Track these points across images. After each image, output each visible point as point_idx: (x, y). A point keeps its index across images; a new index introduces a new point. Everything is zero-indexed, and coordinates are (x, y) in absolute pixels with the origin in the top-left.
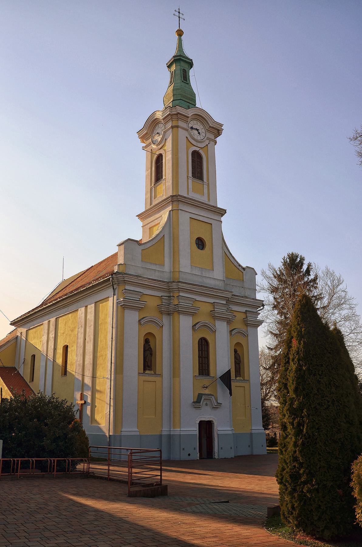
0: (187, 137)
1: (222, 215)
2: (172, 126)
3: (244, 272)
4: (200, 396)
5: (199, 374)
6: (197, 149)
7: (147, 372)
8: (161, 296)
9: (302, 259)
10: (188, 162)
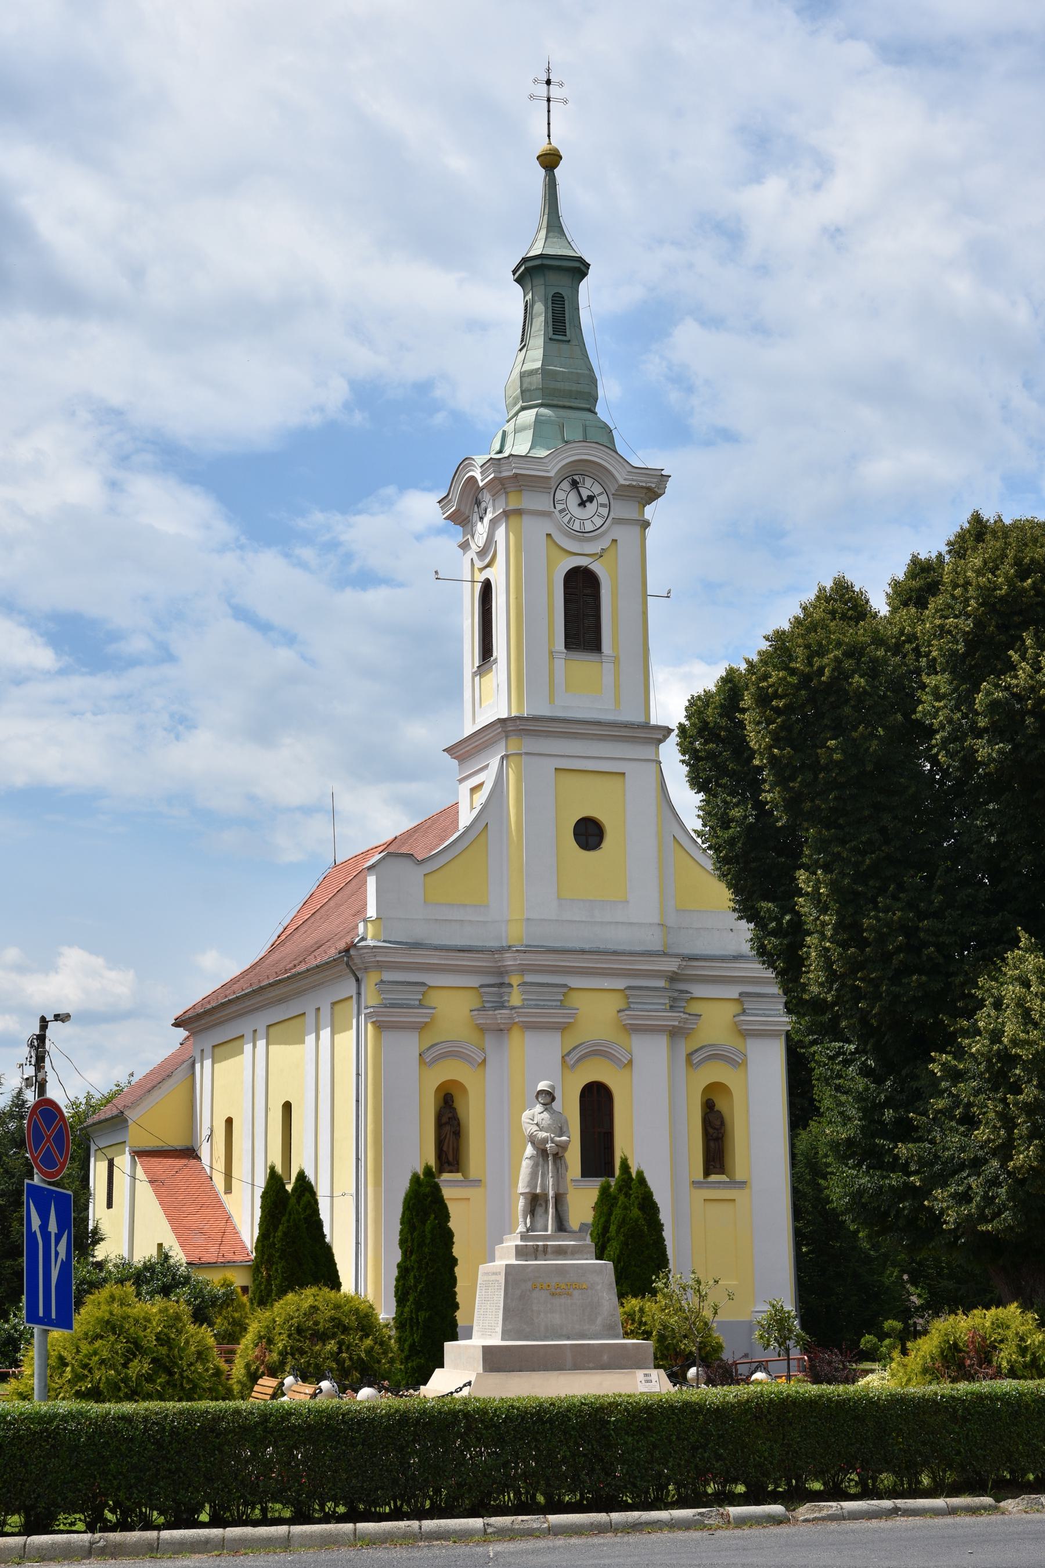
2: (504, 512)
5: (583, 1176)
7: (713, 1178)
8: (482, 986)
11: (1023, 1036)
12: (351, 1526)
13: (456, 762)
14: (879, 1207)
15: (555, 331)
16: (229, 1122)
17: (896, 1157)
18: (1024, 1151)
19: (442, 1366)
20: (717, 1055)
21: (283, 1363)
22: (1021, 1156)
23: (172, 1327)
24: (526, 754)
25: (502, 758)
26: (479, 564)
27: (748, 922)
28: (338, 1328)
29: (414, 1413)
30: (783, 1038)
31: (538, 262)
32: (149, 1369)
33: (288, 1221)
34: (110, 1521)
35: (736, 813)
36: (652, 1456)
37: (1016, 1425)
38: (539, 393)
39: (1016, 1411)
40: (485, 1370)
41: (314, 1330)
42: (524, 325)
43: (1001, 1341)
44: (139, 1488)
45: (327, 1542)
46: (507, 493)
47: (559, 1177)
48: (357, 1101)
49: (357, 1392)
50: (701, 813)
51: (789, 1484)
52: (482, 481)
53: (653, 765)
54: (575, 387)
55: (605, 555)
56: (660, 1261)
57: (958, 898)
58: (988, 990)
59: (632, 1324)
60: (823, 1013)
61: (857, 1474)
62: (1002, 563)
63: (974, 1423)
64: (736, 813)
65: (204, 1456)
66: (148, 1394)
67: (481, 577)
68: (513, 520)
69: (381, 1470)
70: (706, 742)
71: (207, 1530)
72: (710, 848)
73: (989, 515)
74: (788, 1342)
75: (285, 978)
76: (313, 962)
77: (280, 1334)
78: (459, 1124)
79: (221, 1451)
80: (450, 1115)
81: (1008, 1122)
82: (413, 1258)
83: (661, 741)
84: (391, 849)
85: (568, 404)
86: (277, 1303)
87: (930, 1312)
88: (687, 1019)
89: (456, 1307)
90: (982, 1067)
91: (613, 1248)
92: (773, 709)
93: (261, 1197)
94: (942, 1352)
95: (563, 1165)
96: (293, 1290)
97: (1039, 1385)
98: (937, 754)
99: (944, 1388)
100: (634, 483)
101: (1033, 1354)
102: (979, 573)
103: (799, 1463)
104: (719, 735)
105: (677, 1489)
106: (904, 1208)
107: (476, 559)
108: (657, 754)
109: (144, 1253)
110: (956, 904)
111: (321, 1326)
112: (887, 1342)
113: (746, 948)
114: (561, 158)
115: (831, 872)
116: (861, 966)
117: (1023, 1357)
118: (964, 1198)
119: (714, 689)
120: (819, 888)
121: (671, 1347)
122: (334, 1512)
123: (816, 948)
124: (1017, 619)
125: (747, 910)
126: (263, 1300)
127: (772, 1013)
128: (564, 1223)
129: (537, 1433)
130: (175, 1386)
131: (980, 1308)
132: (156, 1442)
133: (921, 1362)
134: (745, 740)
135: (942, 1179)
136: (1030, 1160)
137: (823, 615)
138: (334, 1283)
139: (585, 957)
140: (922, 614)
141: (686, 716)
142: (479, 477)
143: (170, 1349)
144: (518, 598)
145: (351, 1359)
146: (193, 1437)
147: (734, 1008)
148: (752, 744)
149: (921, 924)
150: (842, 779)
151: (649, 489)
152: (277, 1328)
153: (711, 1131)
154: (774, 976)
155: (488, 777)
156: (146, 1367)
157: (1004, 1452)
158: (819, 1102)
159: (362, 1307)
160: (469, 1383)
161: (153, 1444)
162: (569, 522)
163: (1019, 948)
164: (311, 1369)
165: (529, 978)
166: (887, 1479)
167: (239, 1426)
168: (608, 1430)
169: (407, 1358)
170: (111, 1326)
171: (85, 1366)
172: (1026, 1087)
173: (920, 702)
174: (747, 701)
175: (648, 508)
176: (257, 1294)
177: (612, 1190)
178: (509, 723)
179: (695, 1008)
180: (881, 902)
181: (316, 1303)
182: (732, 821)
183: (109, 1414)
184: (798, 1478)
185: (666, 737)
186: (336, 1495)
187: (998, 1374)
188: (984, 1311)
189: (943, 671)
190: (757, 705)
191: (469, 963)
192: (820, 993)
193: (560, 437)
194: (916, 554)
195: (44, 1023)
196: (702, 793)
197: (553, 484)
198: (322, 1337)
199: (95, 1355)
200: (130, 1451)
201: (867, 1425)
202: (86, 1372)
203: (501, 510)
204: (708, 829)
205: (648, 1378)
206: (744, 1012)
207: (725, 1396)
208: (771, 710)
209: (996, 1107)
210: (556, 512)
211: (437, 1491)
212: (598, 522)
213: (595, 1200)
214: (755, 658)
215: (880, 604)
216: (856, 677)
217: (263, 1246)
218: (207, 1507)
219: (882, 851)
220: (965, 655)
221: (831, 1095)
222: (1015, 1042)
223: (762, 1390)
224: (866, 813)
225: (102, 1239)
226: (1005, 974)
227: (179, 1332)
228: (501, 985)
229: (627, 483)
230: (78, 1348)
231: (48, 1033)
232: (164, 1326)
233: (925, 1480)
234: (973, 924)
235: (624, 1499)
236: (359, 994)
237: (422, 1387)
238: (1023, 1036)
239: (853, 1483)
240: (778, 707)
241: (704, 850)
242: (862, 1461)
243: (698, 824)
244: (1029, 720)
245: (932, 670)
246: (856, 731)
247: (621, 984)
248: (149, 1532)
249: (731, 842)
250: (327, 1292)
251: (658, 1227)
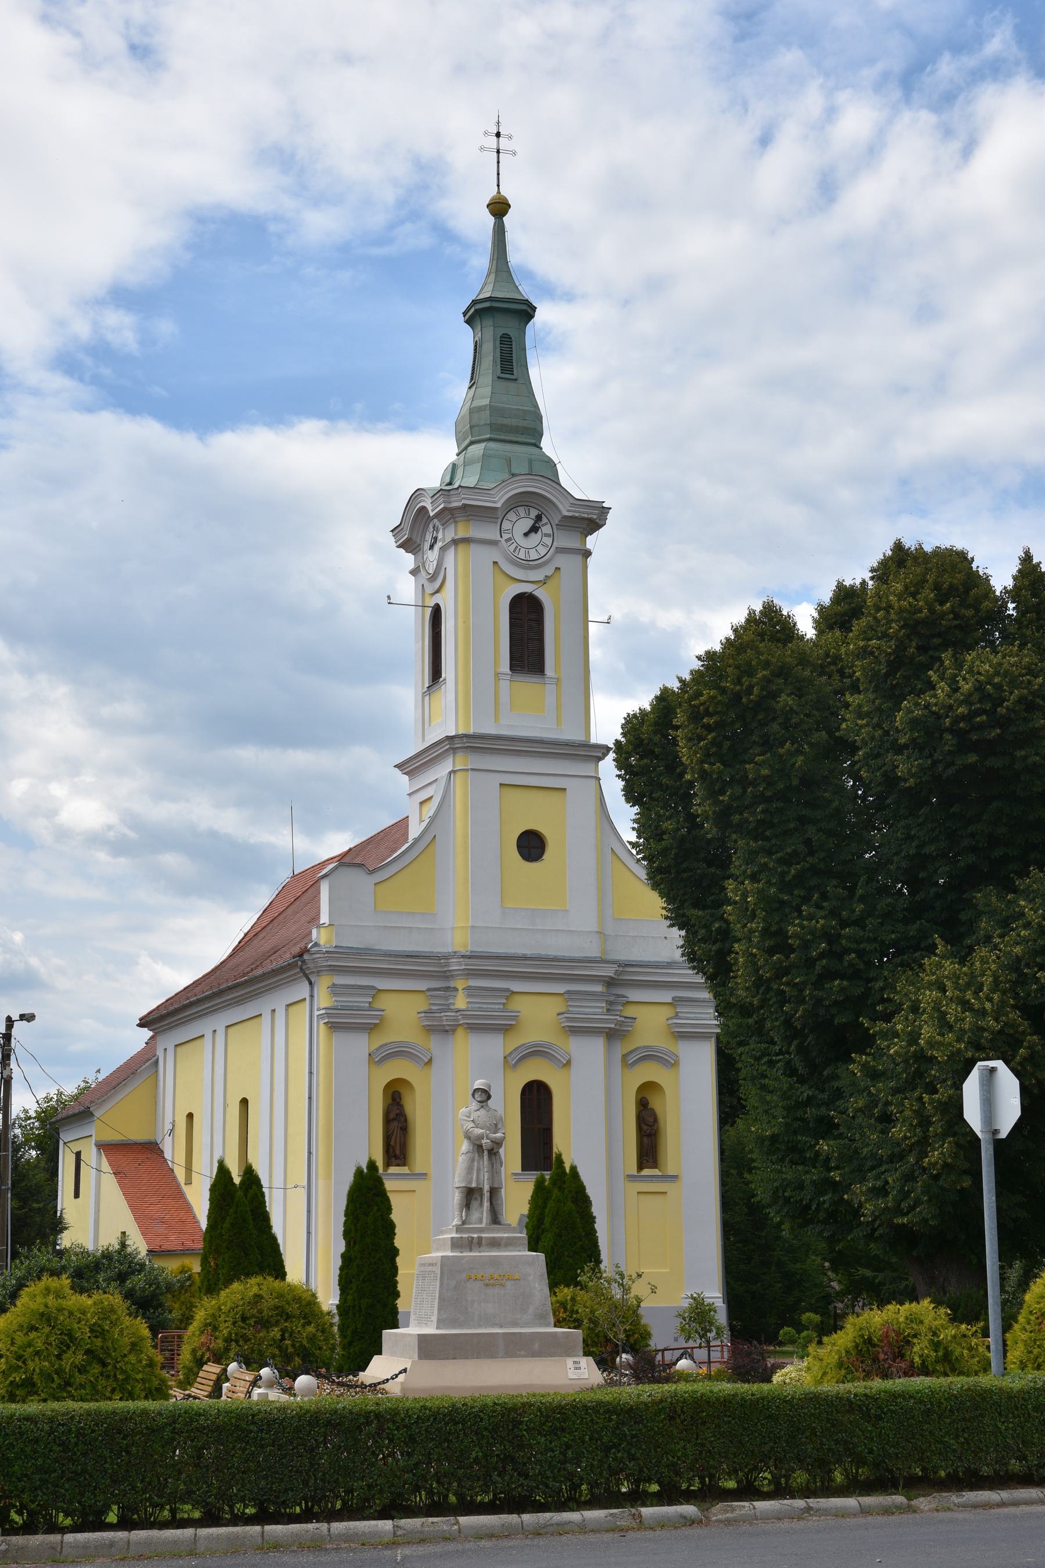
5: (524, 1169)
7: (646, 1172)
8: (429, 990)
11: (939, 1038)
12: (258, 1528)
13: (406, 777)
14: (801, 1200)
15: (503, 371)
16: (190, 1116)
17: (817, 1154)
18: (939, 1147)
19: (380, 1353)
20: (650, 1056)
21: (227, 1349)
22: (936, 1153)
23: (106, 1319)
24: (472, 769)
26: (429, 589)
27: (680, 929)
28: (281, 1316)
29: (326, 1414)
30: (713, 1040)
32: (83, 1360)
33: (236, 1212)
34: (17, 1523)
35: (668, 825)
36: (565, 1455)
37: (929, 1423)
38: (488, 429)
39: (929, 1409)
40: (420, 1357)
41: (257, 1317)
42: (474, 364)
43: (915, 1336)
44: (44, 1490)
45: (235, 1548)
47: (494, 1172)
48: (310, 1098)
49: (294, 1380)
50: (636, 826)
51: (702, 1482)
53: (593, 781)
54: (522, 423)
55: (550, 583)
56: (592, 1254)
57: (879, 907)
58: (906, 994)
59: (565, 1312)
60: (750, 1016)
61: (771, 1472)
62: (923, 588)
63: (887, 1422)
64: (668, 825)
65: (110, 1457)
66: (80, 1384)
67: (431, 602)
68: (461, 548)
69: (290, 1471)
70: (641, 758)
71: (112, 1533)
72: (643, 858)
73: (909, 543)
74: (708, 1334)
75: (242, 982)
76: (269, 967)
77: (226, 1321)
78: (406, 1120)
79: (128, 1452)
80: (398, 1112)
81: (925, 1122)
82: (357, 1247)
83: (600, 759)
84: (346, 860)
85: (514, 439)
86: (222, 1292)
87: (850, 1297)
88: (623, 1022)
89: (397, 1295)
90: (899, 1069)
91: (547, 1239)
92: (703, 726)
93: (210, 1190)
94: (857, 1346)
95: (498, 1161)
96: (239, 1279)
97: (951, 1382)
98: (860, 770)
99: (857, 1387)
100: (577, 514)
101: (945, 1348)
102: (900, 597)
103: (712, 1462)
104: (653, 752)
105: (591, 1490)
106: (824, 1201)
107: (426, 584)
108: (597, 770)
109: (109, 1240)
110: (877, 913)
111: (265, 1313)
112: (805, 1333)
113: (677, 955)
114: (509, 206)
115: (758, 882)
116: (786, 971)
117: (936, 1351)
118: (881, 1191)
119: (649, 708)
120: (747, 897)
121: (602, 1334)
122: (243, 1513)
123: (743, 954)
124: (936, 641)
125: (678, 918)
126: (212, 1285)
127: (703, 1016)
128: (499, 1216)
129: (449, 1433)
130: (108, 1377)
131: (894, 1303)
132: (62, 1444)
133: (836, 1357)
134: (677, 756)
135: (860, 1173)
136: (944, 1156)
137: (752, 636)
138: (279, 1271)
140: (846, 637)
141: (622, 734)
142: (430, 508)
143: (104, 1340)
144: (466, 622)
145: (293, 1346)
146: (100, 1438)
147: (666, 1012)
148: (684, 759)
149: (843, 932)
150: (768, 793)
151: (591, 520)
152: (223, 1316)
153: (645, 1127)
154: (703, 981)
155: (436, 792)
156: (80, 1358)
157: (916, 1449)
158: (745, 1100)
159: (304, 1296)
160: (405, 1370)
161: (59, 1445)
162: (514, 551)
163: (936, 955)
164: (255, 1355)
166: (800, 1477)
167: (147, 1428)
168: (521, 1430)
169: (350, 1343)
170: (46, 1317)
171: (19, 1357)
172: (941, 1087)
173: (844, 720)
174: (680, 718)
175: (589, 538)
176: (205, 1283)
177: (547, 1183)
178: (457, 740)
179: (630, 1011)
180: (805, 910)
181: (261, 1292)
182: (664, 833)
183: (15, 1415)
184: (711, 1477)
185: (605, 755)
186: (244, 1496)
187: (911, 1371)
188: (898, 1306)
189: (866, 690)
190: (689, 722)
192: (747, 997)
193: (507, 471)
194: (841, 581)
195: (10, 1022)
196: (637, 807)
197: (499, 514)
198: (265, 1324)
199: (30, 1347)
200: (35, 1453)
201: (781, 1424)
202: (20, 1364)
204: (642, 840)
205: (578, 1366)
207: (639, 1395)
208: (702, 727)
209: (913, 1105)
210: (503, 540)
211: (350, 1491)
212: (543, 551)
213: (531, 1193)
214: (687, 677)
215: (806, 625)
216: (784, 697)
217: (211, 1236)
218: (115, 1508)
219: (807, 862)
220: (887, 675)
221: (757, 1094)
222: (932, 1044)
223: (676, 1389)
224: (792, 825)
225: (66, 1228)
226: (923, 980)
227: (113, 1324)
228: (447, 989)
229: (570, 514)
230: (13, 1339)
231: (14, 1032)
232: (99, 1318)
233: (838, 1477)
234: (893, 932)
235: (537, 1498)
236: (312, 996)
237: (361, 1373)
238: (939, 1038)
239: (766, 1482)
240: (708, 724)
241: (638, 860)
242: (776, 1460)
243: (633, 837)
244: (948, 736)
245: (855, 689)
246: (783, 748)
247: (561, 988)
248: (52, 1535)
249: (664, 852)
250: (271, 1283)
251: (591, 1220)
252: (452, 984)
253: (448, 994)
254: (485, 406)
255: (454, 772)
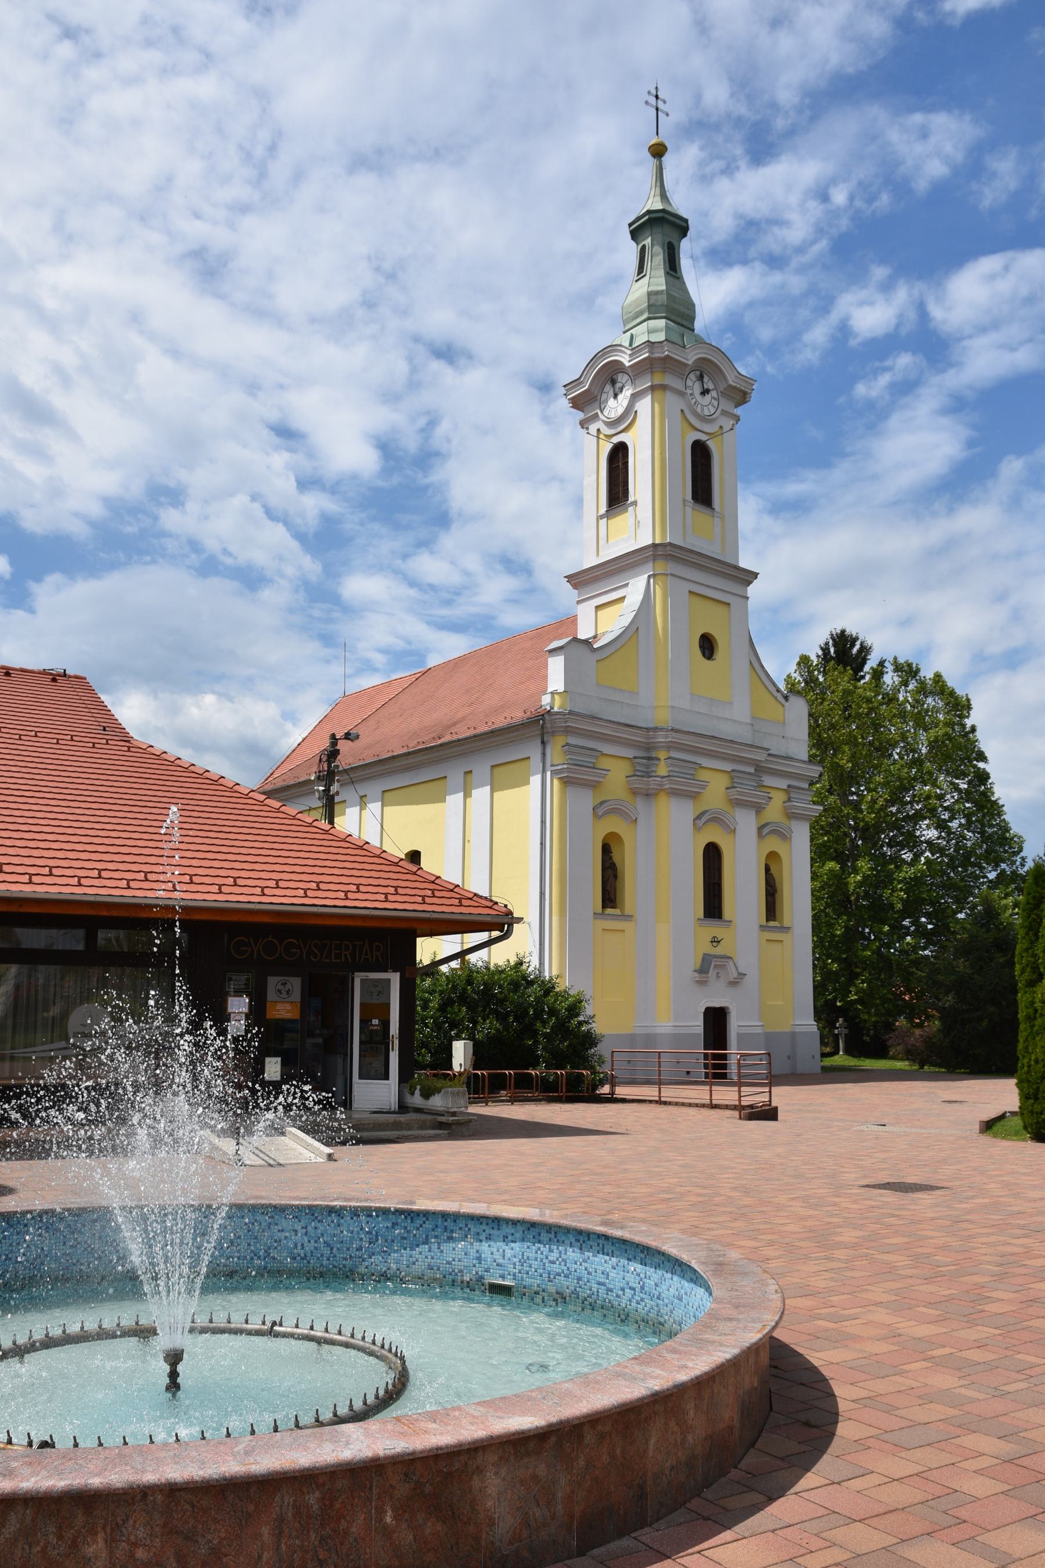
0: (682, 411)
1: (749, 583)
3: (786, 704)
4: (707, 959)
5: (705, 916)
6: (703, 437)
7: (609, 911)
8: (635, 758)
9: (865, 650)
10: (684, 466)
24: (672, 575)
25: (649, 577)
31: (660, 215)
46: (652, 373)
52: (630, 361)
68: (658, 394)
139: (713, 741)
144: (663, 453)
165: (674, 754)
178: (660, 548)
191: (630, 737)
203: (650, 384)
206: (789, 800)
212: (713, 411)
228: (649, 758)
229: (735, 384)
247: (728, 767)
252: (654, 755)
253: (651, 762)
254: (662, 291)
255: (654, 575)
